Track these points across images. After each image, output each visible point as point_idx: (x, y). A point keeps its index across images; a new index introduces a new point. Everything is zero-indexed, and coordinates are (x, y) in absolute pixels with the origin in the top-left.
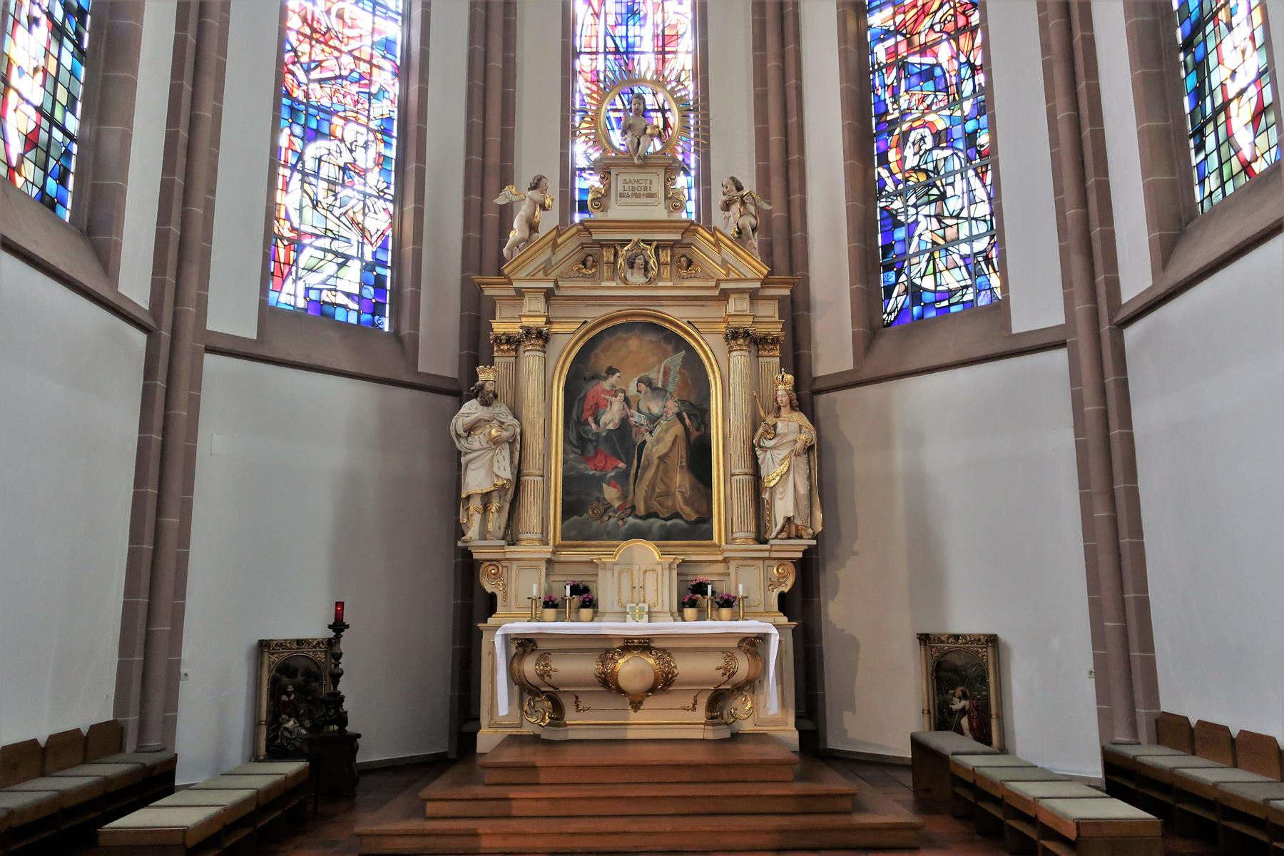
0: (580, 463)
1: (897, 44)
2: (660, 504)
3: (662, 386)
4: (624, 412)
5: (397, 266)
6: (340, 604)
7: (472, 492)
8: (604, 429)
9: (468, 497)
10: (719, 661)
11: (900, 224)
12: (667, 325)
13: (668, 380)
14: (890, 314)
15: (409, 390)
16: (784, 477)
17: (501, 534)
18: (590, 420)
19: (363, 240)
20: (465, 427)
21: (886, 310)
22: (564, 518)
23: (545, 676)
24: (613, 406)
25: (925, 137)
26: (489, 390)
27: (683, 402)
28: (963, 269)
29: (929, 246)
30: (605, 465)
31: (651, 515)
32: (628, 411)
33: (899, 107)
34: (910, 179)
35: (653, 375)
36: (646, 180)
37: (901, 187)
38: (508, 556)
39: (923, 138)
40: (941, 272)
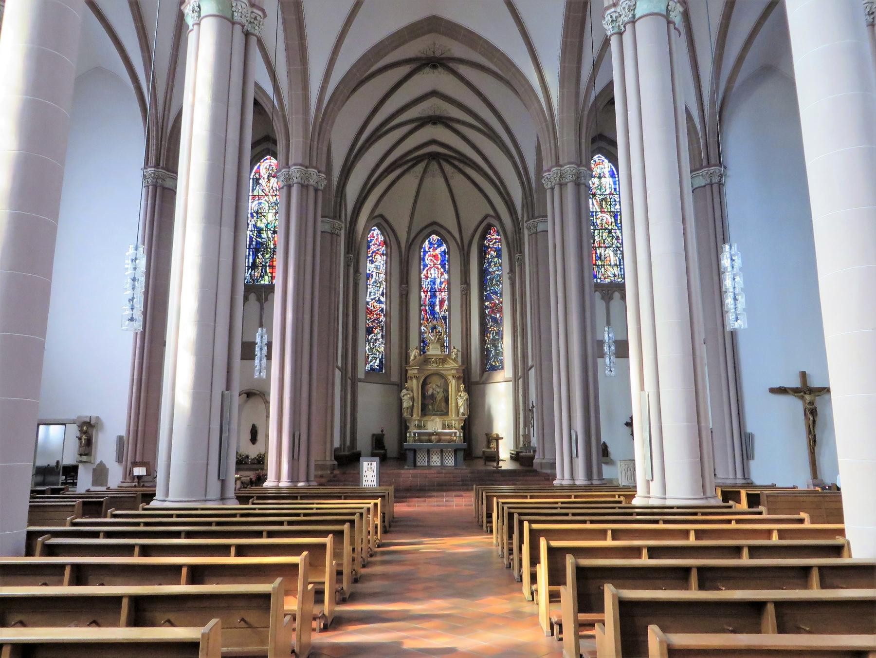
35: (437, 384)
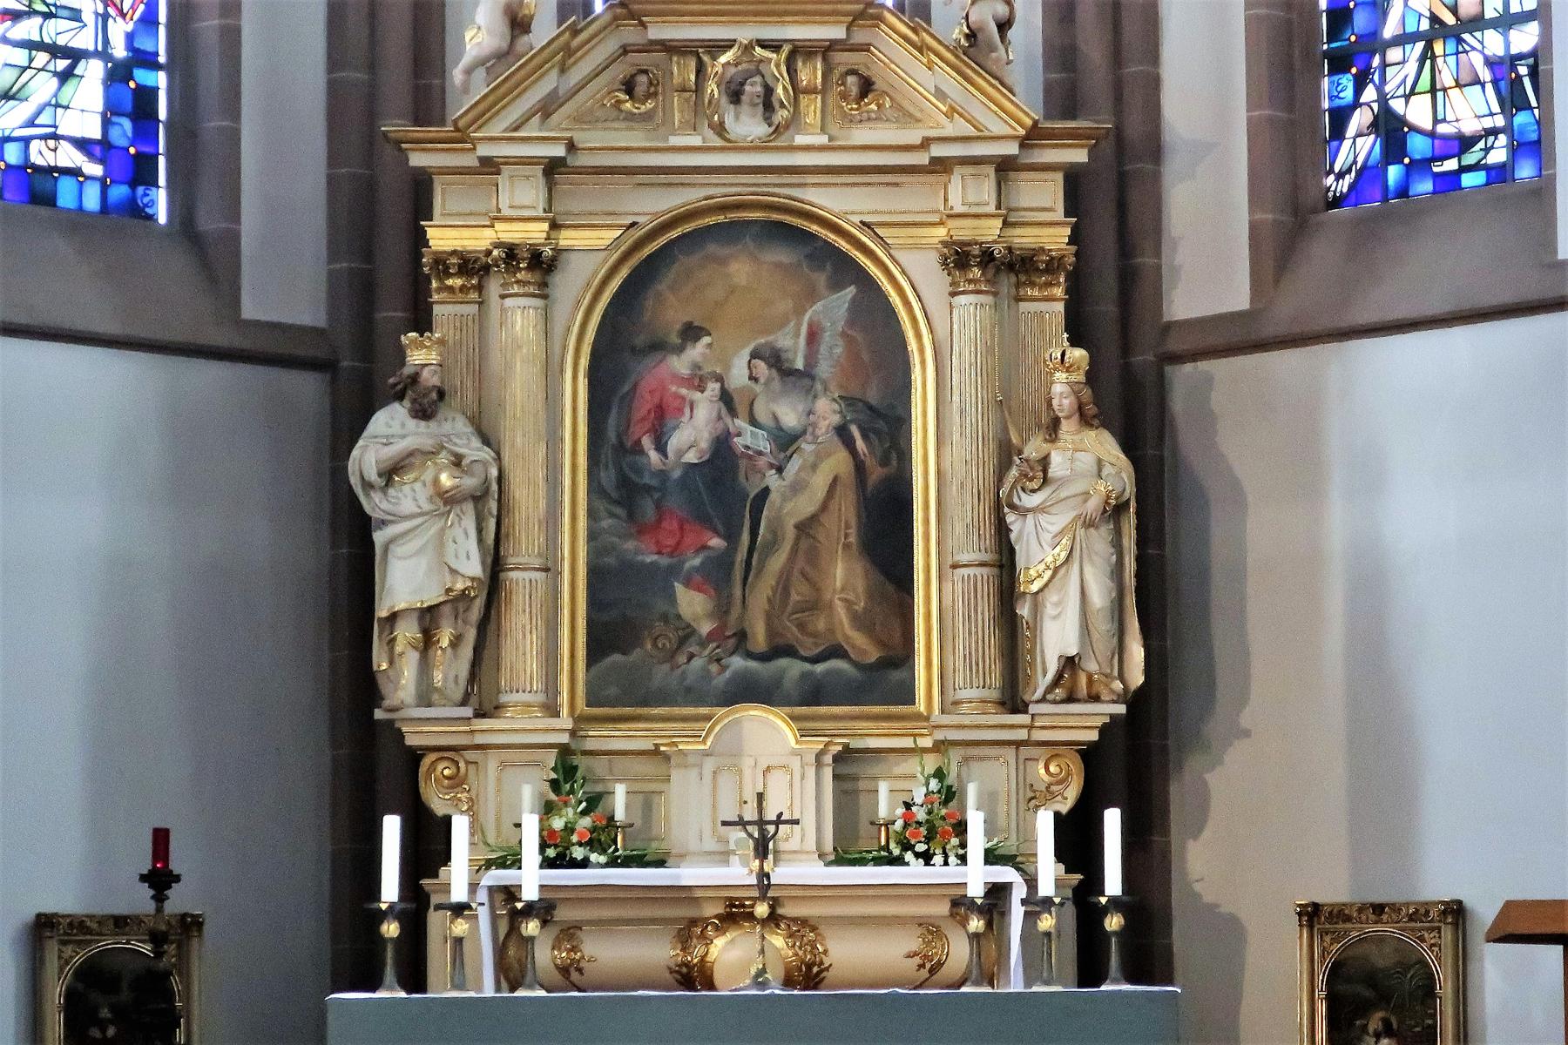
0: (626, 536)
2: (802, 626)
3: (805, 366)
5: (182, 63)
6: (161, 838)
8: (678, 463)
10: (911, 941)
12: (814, 228)
15: (249, 367)
16: (1062, 571)
17: (458, 694)
18: (647, 442)
19: (106, 8)
20: (382, 466)
23: (572, 970)
24: (695, 411)
27: (849, 401)
28: (1489, 87)
29: (1425, 25)
30: (678, 544)
31: (781, 650)
32: (728, 420)
38: (480, 739)
40: (1445, 90)
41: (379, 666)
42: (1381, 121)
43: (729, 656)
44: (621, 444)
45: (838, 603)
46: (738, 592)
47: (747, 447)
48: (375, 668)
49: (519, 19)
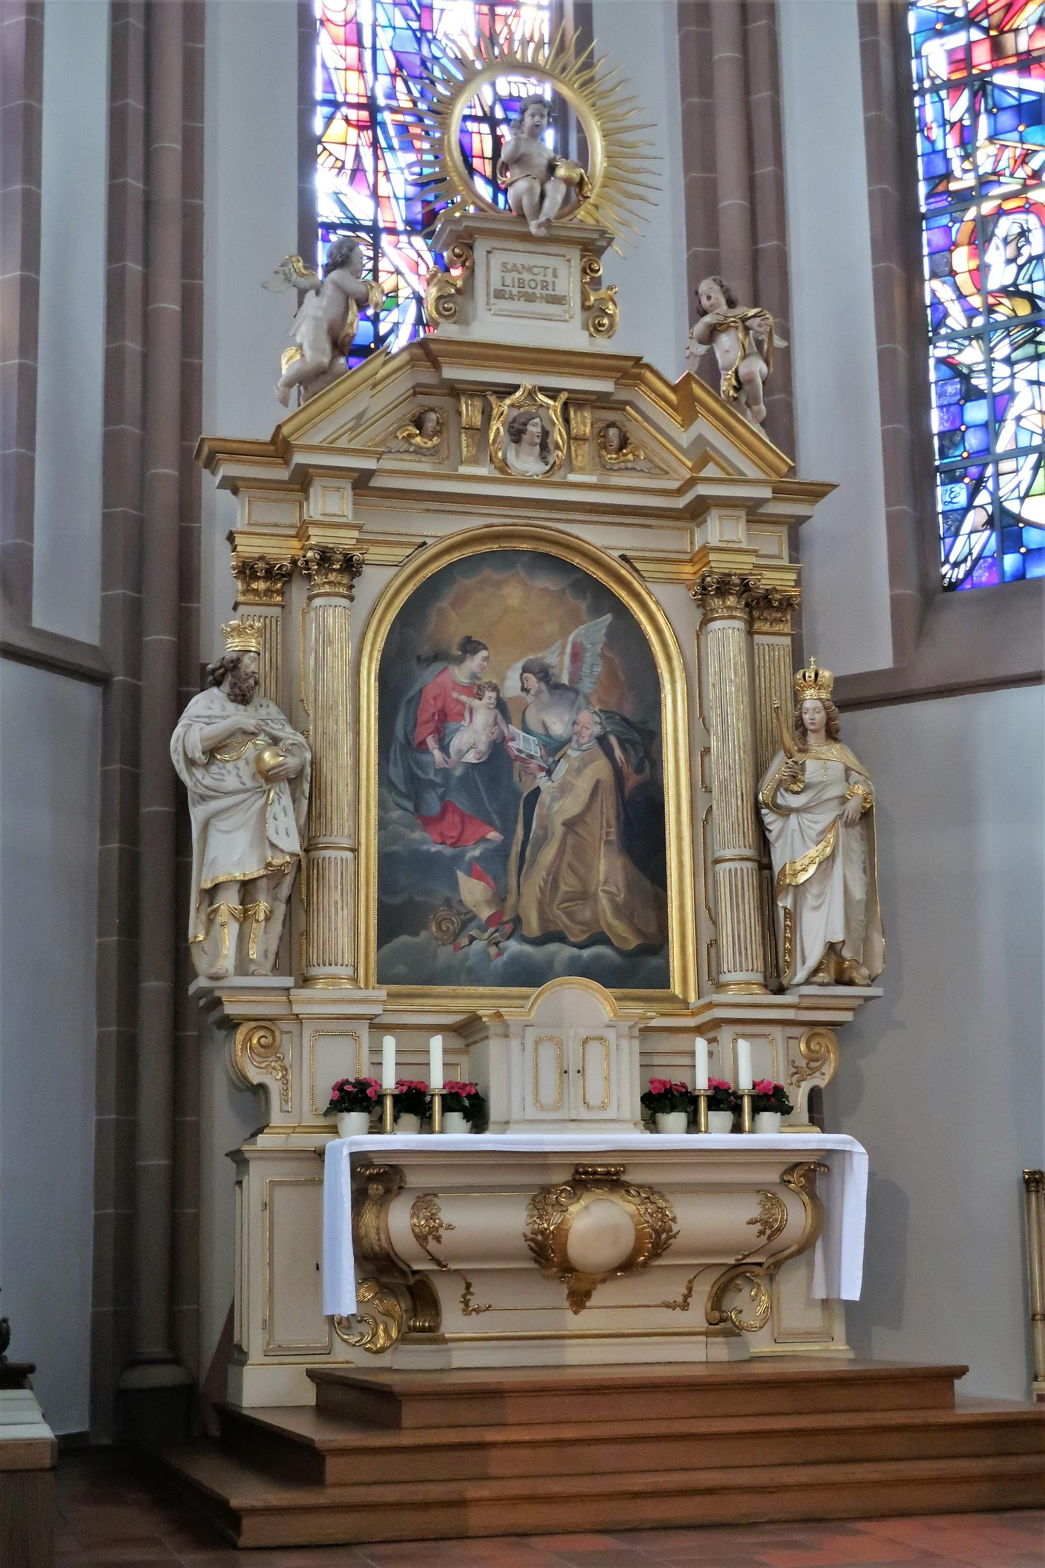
0: (412, 828)
1: (969, 46)
2: (570, 915)
3: (570, 681)
4: (496, 730)
7: (221, 879)
9: (211, 893)
10: (748, 1209)
11: (980, 395)
12: (577, 561)
13: (580, 669)
14: (956, 565)
16: (824, 866)
18: (431, 742)
21: (947, 556)
22: (381, 942)
23: (430, 1238)
25: (1029, 231)
26: (249, 670)
27: (608, 714)
31: (551, 936)
32: (503, 726)
33: (976, 168)
34: (997, 308)
35: (551, 658)
36: (546, 268)
37: (978, 322)
39: (1023, 233)
41: (196, 937)
42: (997, 518)
43: (508, 939)
44: (408, 742)
45: (601, 894)
46: (513, 881)
47: (520, 751)
48: (191, 939)
49: (340, 340)
